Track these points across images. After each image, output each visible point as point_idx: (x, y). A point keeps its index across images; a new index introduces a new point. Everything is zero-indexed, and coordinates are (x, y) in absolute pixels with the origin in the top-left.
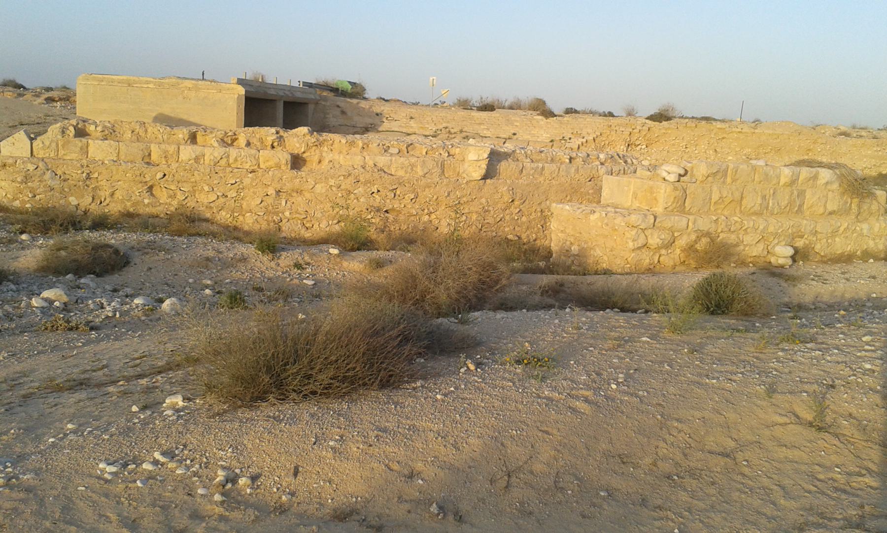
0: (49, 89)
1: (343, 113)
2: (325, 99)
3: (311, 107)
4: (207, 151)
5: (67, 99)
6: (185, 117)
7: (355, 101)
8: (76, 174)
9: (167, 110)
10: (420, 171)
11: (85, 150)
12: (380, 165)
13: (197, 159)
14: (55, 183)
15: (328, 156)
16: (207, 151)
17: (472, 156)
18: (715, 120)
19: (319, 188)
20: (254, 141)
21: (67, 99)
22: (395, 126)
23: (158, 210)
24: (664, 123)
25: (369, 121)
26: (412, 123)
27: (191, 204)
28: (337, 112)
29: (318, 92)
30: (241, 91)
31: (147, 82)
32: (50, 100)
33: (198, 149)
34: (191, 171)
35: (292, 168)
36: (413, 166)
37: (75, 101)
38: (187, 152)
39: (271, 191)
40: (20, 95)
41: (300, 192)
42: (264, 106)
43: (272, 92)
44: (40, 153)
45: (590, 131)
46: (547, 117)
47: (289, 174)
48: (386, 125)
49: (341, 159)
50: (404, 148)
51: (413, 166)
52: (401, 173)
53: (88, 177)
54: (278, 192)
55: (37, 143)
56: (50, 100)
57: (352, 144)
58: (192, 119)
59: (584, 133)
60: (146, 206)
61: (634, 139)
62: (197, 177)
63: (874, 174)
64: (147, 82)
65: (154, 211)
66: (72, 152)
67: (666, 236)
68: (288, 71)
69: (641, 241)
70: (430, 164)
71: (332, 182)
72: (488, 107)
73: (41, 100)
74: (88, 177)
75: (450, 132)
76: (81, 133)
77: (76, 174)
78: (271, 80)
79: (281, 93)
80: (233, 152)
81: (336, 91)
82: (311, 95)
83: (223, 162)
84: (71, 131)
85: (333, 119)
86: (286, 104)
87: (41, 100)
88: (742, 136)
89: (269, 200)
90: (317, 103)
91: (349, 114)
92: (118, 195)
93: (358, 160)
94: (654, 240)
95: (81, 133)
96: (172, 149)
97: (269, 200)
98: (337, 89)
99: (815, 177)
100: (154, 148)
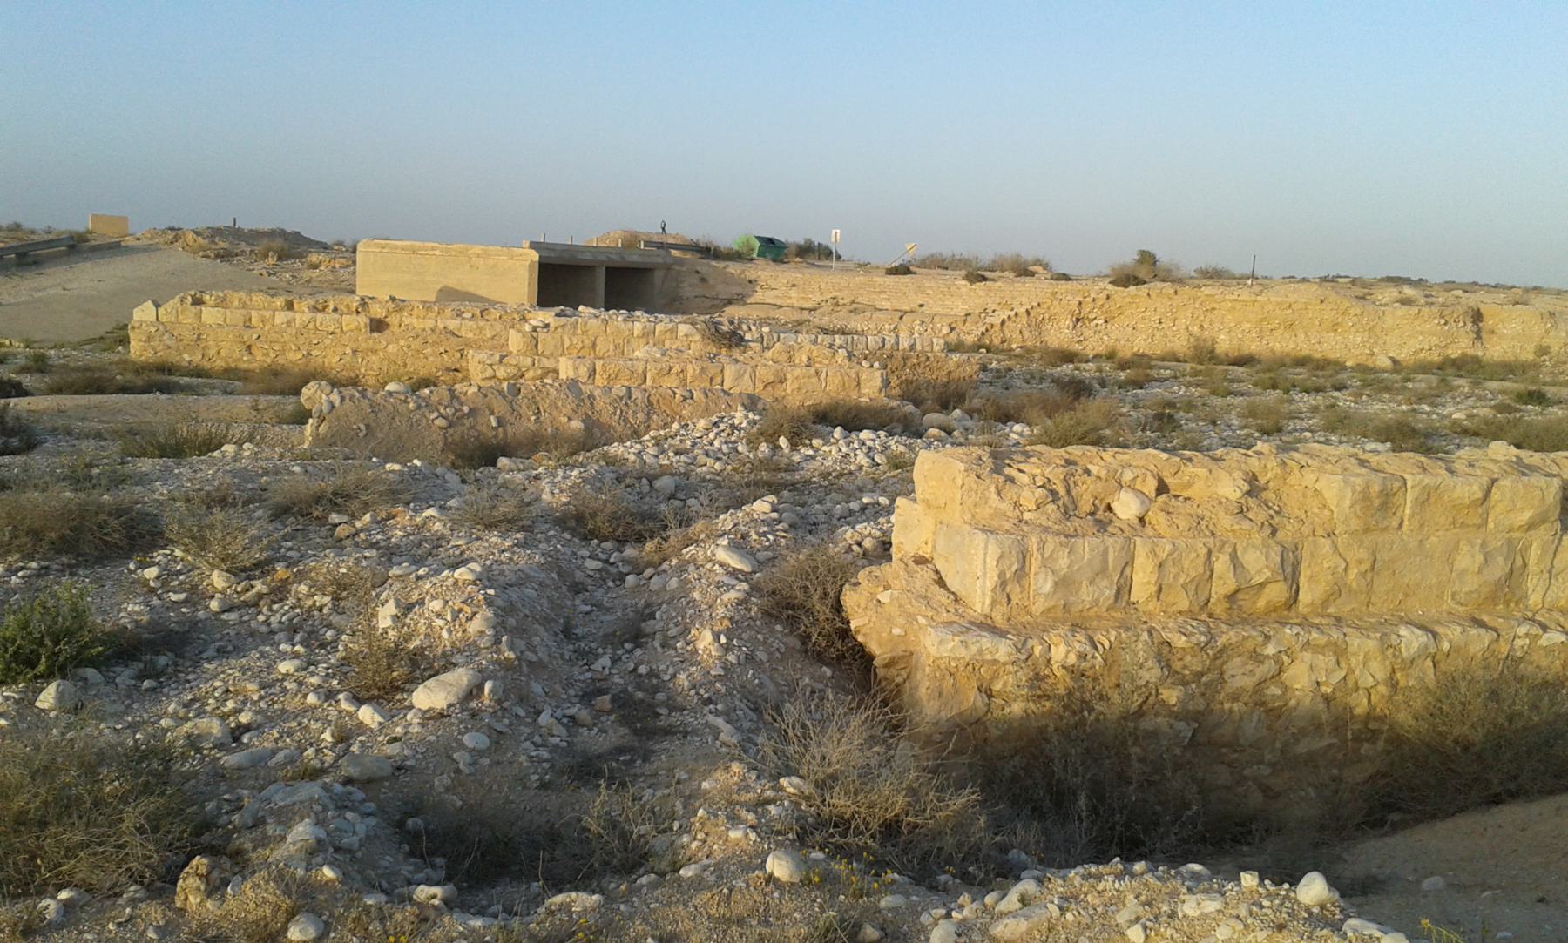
1: (703, 280)
2: (680, 262)
3: (658, 276)
4: (298, 316)
6: (472, 290)
7: (721, 265)
8: (188, 335)
9: (452, 282)
11: (199, 316)
12: (450, 328)
13: (288, 323)
14: (172, 343)
15: (407, 320)
22: (769, 297)
23: (254, 366)
24: (1132, 288)
25: (739, 290)
26: (793, 293)
27: (281, 361)
28: (695, 279)
30: (535, 256)
31: (433, 249)
33: (290, 314)
34: (281, 332)
35: (372, 331)
36: (481, 329)
38: (281, 317)
39: (348, 350)
41: (375, 352)
42: (563, 279)
43: (588, 256)
44: (163, 318)
45: (1024, 300)
46: (972, 282)
48: (758, 296)
50: (478, 312)
51: (481, 329)
52: (470, 335)
53: (199, 338)
54: (354, 352)
55: (161, 311)
58: (480, 293)
59: (1016, 303)
60: (245, 362)
62: (286, 338)
63: (1435, 358)
64: (433, 249)
65: (251, 366)
66: (189, 316)
67: (514, 371)
68: (593, 228)
69: (489, 372)
71: (402, 343)
72: (903, 270)
74: (199, 338)
75: (837, 304)
77: (188, 335)
78: (88, 265)
79: (602, 258)
80: (320, 317)
81: (708, 252)
82: (657, 258)
83: (311, 326)
85: (688, 289)
89: (348, 358)
90: (668, 268)
91: (711, 282)
92: (223, 353)
93: (430, 323)
96: (268, 314)
97: (348, 358)
98: (708, 249)
100: (254, 314)
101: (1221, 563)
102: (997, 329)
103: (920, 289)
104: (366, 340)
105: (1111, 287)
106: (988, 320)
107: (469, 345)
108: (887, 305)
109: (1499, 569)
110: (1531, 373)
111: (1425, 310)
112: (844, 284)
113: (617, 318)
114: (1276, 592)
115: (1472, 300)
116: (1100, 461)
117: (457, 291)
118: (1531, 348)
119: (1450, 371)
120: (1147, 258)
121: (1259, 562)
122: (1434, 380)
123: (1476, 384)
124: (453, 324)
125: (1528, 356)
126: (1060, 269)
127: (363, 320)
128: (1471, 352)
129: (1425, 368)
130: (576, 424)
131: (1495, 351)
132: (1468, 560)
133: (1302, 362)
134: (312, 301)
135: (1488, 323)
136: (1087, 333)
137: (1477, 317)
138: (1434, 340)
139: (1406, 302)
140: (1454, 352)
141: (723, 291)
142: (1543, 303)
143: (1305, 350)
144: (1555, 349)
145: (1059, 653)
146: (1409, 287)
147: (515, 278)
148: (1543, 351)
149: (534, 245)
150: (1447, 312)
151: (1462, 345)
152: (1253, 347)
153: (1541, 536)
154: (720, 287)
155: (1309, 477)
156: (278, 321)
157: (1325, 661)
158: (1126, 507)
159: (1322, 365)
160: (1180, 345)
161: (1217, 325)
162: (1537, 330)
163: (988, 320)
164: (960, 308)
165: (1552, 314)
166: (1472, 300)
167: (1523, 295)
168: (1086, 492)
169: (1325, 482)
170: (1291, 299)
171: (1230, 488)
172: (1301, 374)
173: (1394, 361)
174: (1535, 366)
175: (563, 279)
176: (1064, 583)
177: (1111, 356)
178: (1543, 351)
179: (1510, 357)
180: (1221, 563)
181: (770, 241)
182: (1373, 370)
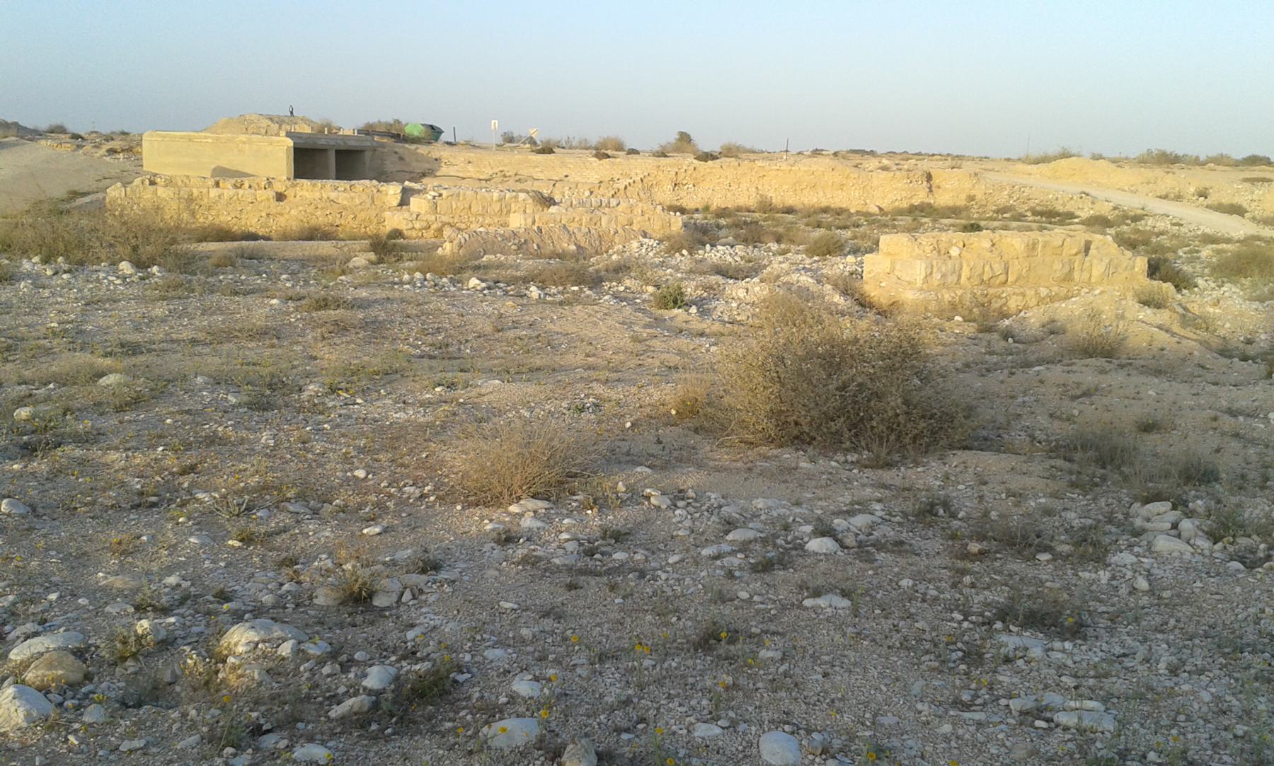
0: (109, 138)
1: (401, 159)
2: (383, 145)
3: (368, 155)
4: (225, 192)
5: (130, 150)
6: (240, 169)
7: (413, 147)
9: (224, 163)
10: (358, 202)
11: (155, 192)
16: (225, 192)
17: (391, 192)
18: (769, 156)
19: (293, 212)
20: (254, 185)
21: (130, 150)
22: (452, 171)
24: (710, 162)
25: (428, 166)
26: (470, 167)
29: (376, 138)
30: (290, 143)
31: (206, 137)
32: (112, 151)
37: (141, 153)
39: (264, 214)
40: (79, 147)
41: (282, 214)
42: (312, 158)
47: (273, 203)
48: (444, 170)
49: (307, 194)
56: (112, 151)
57: (314, 185)
59: (633, 174)
61: (680, 178)
63: (905, 205)
64: (206, 137)
67: (425, 224)
69: (410, 226)
70: (364, 197)
73: (103, 151)
76: (152, 183)
78: (383, 120)
79: (332, 143)
80: (241, 192)
82: (366, 142)
84: (147, 182)
85: (390, 166)
86: (338, 152)
87: (103, 151)
88: (780, 174)
89: (262, 220)
91: (407, 159)
93: (317, 195)
94: (417, 226)
95: (152, 183)
96: (205, 191)
99: (516, 197)
101: (987, 268)
102: (622, 192)
103: (563, 164)
104: (275, 207)
105: (696, 162)
106: (616, 186)
107: (345, 208)
108: (541, 176)
109: (1066, 270)
110: (964, 214)
111: (898, 173)
112: (506, 161)
113: (343, 184)
114: (1002, 278)
115: (925, 165)
116: (944, 237)
117: (229, 170)
118: (963, 196)
119: (917, 213)
120: (685, 138)
121: (998, 268)
122: (909, 219)
123: (935, 221)
124: (333, 195)
125: (961, 202)
126: (628, 146)
127: (271, 194)
128: (927, 201)
129: (901, 212)
130: (573, 247)
131: (943, 199)
132: (1057, 266)
133: (825, 210)
134: (233, 181)
135: (935, 181)
136: (683, 194)
137: (929, 177)
138: (904, 194)
139: (885, 169)
140: (916, 202)
141: (418, 167)
142: (969, 167)
143: (824, 204)
144: (979, 197)
145: (947, 296)
146: (899, 158)
147: (276, 156)
148: (971, 198)
149: (289, 134)
150: (911, 174)
151: (920, 197)
152: (791, 201)
153: (1079, 257)
154: (414, 164)
155: (1009, 240)
156: (212, 195)
157: (1020, 298)
158: (954, 252)
159: (840, 212)
160: (752, 202)
161: (767, 187)
162: (967, 185)
163: (616, 186)
164: (594, 178)
165: (976, 174)
166: (925, 165)
167: (956, 160)
168: (943, 246)
169: (1014, 242)
170: (814, 168)
171: (987, 245)
172: (828, 218)
173: (881, 209)
174: (967, 208)
175: (312, 158)
176: (944, 276)
177: (707, 209)
178: (971, 198)
179: (951, 203)
180: (987, 268)
181: (432, 127)
182: (871, 215)
